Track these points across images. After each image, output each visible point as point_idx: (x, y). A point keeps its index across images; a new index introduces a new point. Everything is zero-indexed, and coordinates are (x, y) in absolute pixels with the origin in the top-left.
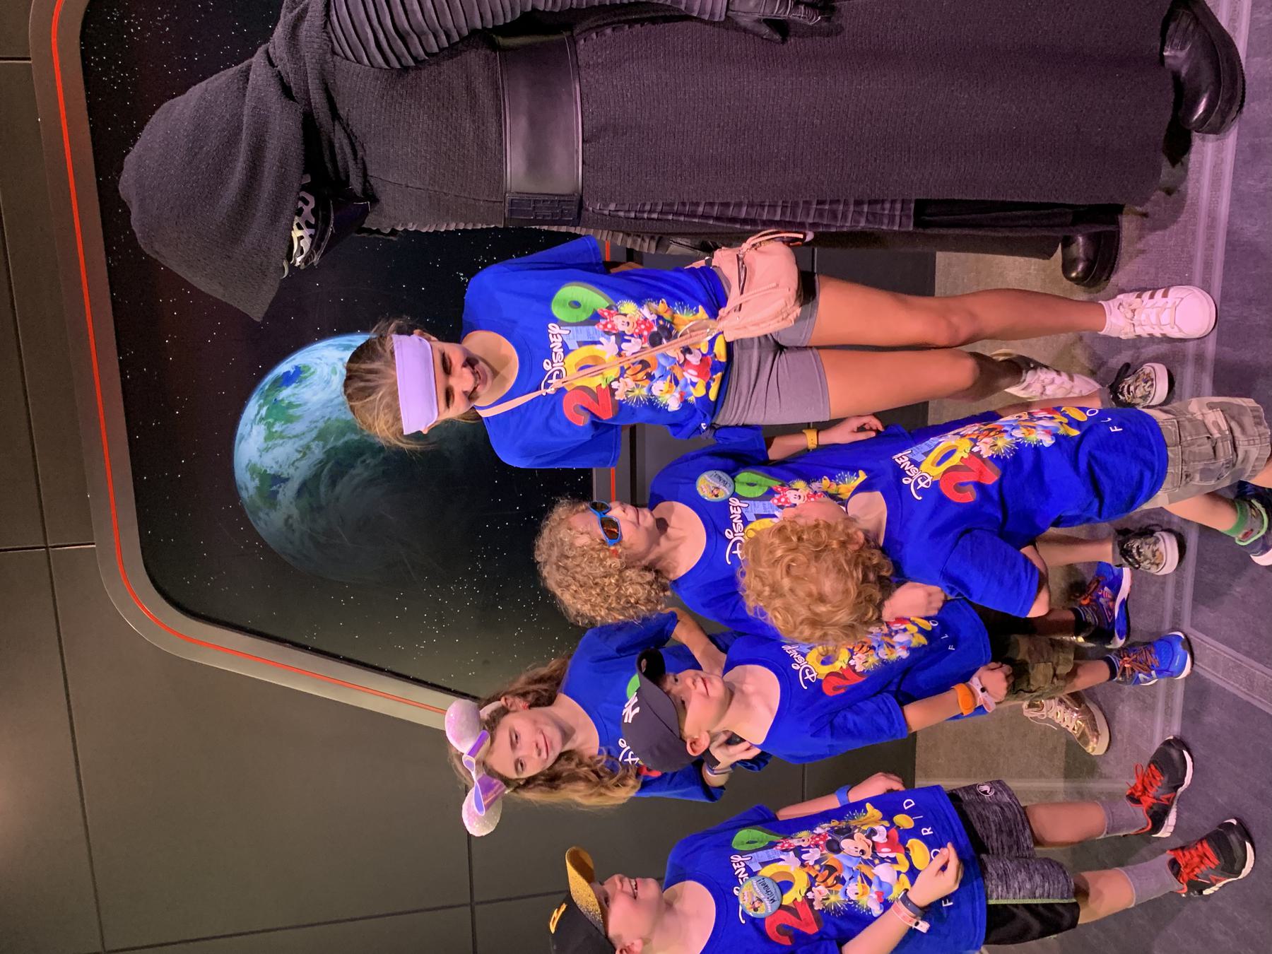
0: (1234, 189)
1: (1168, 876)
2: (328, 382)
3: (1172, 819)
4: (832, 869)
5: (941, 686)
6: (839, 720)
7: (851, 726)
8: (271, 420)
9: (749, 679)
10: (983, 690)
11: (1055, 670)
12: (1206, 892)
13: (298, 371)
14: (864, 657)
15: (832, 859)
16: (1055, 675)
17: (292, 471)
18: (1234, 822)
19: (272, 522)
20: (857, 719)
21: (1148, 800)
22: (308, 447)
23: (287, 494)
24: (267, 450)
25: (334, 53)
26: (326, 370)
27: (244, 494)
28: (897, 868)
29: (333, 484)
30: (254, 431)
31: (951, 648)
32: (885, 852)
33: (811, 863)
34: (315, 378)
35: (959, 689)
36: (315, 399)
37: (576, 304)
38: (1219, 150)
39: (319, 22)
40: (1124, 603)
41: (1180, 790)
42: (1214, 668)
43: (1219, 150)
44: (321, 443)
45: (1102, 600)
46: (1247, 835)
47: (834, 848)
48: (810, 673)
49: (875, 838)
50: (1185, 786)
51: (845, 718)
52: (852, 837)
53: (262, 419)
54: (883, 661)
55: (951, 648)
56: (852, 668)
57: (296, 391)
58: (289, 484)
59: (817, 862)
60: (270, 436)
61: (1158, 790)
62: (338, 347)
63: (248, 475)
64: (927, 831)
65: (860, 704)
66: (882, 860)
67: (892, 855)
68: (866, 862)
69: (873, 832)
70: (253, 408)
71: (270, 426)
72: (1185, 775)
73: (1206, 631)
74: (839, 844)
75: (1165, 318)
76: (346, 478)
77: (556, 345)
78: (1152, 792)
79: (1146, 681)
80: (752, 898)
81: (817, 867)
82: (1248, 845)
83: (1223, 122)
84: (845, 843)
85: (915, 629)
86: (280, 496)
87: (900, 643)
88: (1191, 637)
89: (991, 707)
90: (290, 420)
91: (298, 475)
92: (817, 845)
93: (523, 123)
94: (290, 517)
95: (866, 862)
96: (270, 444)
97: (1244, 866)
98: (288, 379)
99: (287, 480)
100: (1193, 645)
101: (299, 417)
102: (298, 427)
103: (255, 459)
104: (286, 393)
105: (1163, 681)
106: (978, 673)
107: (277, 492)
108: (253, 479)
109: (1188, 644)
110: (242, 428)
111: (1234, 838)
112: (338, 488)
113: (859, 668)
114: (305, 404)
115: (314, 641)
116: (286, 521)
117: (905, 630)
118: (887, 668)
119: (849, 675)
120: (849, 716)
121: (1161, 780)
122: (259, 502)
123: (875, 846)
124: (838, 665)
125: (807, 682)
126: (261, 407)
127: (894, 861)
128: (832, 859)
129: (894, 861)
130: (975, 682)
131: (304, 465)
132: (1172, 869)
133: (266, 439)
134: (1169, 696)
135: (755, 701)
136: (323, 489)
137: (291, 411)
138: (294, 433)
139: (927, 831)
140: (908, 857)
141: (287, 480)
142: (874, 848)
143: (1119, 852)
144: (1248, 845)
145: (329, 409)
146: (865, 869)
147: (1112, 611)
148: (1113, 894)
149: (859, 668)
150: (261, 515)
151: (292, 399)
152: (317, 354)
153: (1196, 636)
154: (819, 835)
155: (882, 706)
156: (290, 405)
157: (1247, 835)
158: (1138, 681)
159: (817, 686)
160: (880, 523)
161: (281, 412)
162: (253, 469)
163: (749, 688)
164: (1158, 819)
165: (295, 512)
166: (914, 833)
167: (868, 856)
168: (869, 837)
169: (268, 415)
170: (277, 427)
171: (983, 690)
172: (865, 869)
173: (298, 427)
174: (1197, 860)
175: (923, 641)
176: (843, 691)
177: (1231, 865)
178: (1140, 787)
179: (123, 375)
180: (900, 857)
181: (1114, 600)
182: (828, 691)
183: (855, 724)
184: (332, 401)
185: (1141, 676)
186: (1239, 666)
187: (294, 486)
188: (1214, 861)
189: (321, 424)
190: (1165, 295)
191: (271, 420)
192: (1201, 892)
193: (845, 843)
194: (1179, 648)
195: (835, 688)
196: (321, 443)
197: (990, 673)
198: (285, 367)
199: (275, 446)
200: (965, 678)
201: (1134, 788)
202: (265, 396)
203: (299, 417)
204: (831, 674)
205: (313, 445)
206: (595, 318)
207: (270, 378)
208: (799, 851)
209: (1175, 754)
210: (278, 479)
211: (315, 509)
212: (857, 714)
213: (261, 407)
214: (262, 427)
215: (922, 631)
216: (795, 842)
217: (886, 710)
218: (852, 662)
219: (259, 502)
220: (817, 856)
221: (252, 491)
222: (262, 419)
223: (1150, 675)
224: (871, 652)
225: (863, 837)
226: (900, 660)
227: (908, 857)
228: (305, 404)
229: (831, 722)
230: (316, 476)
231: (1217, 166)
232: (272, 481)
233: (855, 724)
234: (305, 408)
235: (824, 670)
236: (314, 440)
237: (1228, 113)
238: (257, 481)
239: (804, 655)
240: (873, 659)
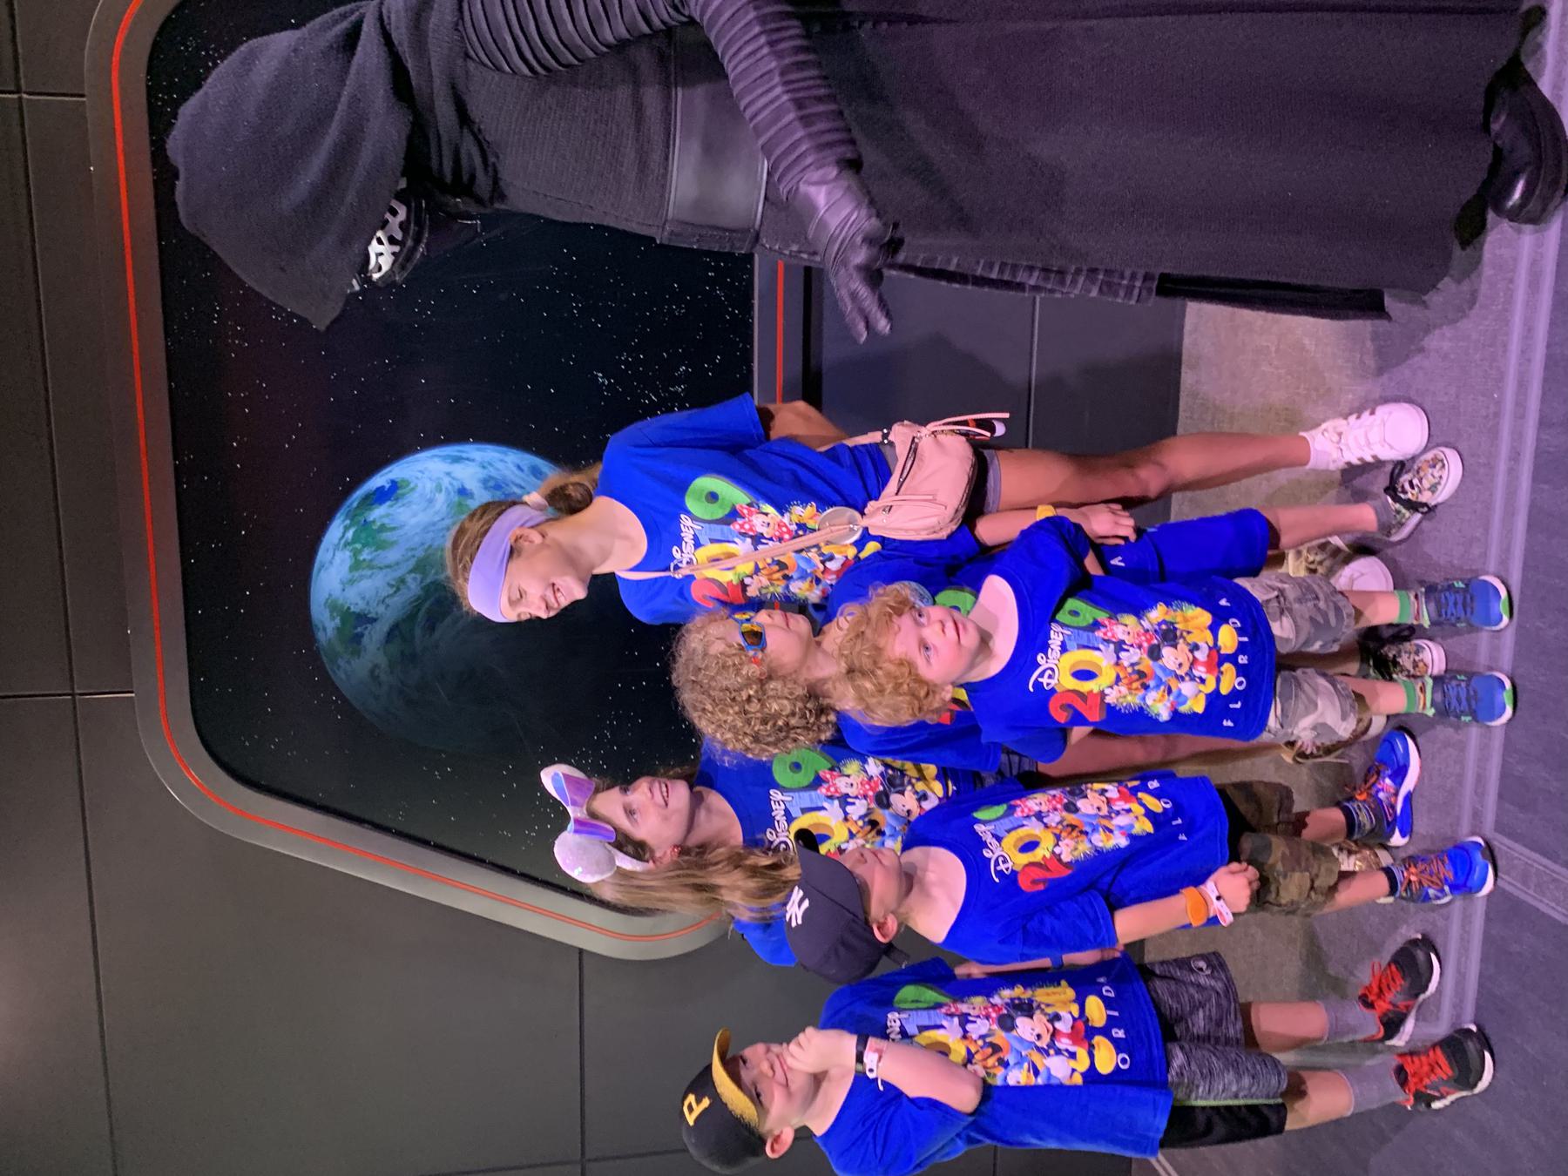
0: (1557, 292)
1: (1392, 1084)
2: (431, 501)
3: (1409, 1025)
4: (996, 1049)
5: (1167, 889)
6: (1033, 925)
7: (1047, 932)
8: (358, 546)
9: (931, 866)
10: (1218, 898)
11: (1312, 881)
12: (1436, 1105)
13: (395, 485)
14: (1072, 843)
15: (1000, 1037)
16: (1312, 888)
17: (381, 609)
18: (1474, 1028)
19: (357, 670)
20: (1056, 923)
21: (1382, 1006)
22: (402, 581)
23: (374, 637)
24: (352, 582)
25: (467, 56)
26: (429, 486)
27: (320, 636)
28: (1072, 1064)
29: (431, 626)
30: (337, 560)
31: (1183, 837)
32: (1064, 1043)
33: (974, 1036)
34: (414, 496)
35: (1189, 893)
36: (413, 521)
37: (713, 497)
38: (1539, 245)
39: (450, 18)
40: (1408, 798)
41: (1422, 997)
42: (1525, 883)
43: (1539, 245)
44: (419, 576)
45: (1381, 795)
46: (1485, 1042)
47: (1007, 1024)
48: (1005, 862)
49: (1058, 1025)
50: (1428, 993)
51: (1042, 922)
52: (1031, 1017)
53: (347, 544)
54: (1099, 851)
55: (1183, 837)
56: (1057, 857)
57: (391, 511)
58: (378, 626)
59: (982, 1037)
60: (356, 565)
61: (1395, 996)
62: (444, 458)
63: (327, 614)
64: (1119, 1033)
65: (1062, 905)
66: (1058, 1052)
67: (1072, 1049)
68: (1039, 1049)
69: (1056, 1017)
70: (337, 530)
71: (356, 553)
72: (1429, 980)
73: (1512, 835)
74: (1013, 1019)
75: (1375, 436)
76: (448, 620)
77: (687, 536)
78: (1389, 997)
79: (1438, 898)
80: (1058, 669)
81: (980, 1043)
82: (1487, 1055)
83: (1544, 210)
84: (1021, 1022)
85: (1142, 811)
86: (365, 640)
87: (1120, 827)
88: (1495, 844)
89: (1227, 918)
90: (381, 546)
91: (388, 615)
92: (988, 1017)
93: (696, 147)
94: (376, 666)
95: (1039, 1049)
96: (356, 574)
97: (1480, 1078)
98: (382, 496)
99: (375, 620)
100: (1496, 853)
101: (394, 543)
102: (392, 555)
103: (337, 592)
104: (378, 513)
105: (1459, 903)
106: (1213, 877)
107: (362, 635)
108: (333, 618)
109: (1490, 853)
110: (323, 554)
111: (1471, 1046)
112: (437, 634)
113: (1066, 858)
114: (402, 526)
115: (399, 822)
116: (372, 672)
117: (1129, 811)
118: (1101, 858)
119: (1054, 866)
120: (1048, 920)
121: (1401, 984)
122: (339, 648)
123: (1194, 662)
124: (1039, 854)
125: (1000, 873)
126: (346, 529)
127: (1073, 1055)
128: (1000, 1037)
129: (1203, 681)
130: (1210, 888)
131: (398, 600)
132: (1398, 1078)
133: (353, 568)
134: (1466, 919)
135: (936, 892)
136: (418, 632)
137: (384, 536)
138: (387, 562)
139: (1119, 1033)
140: (1091, 1056)
141: (375, 620)
142: (1053, 1035)
143: (1334, 1050)
144: (1487, 1055)
145: (431, 535)
146: (1037, 1058)
147: (1393, 807)
148: (1327, 1101)
149: (1066, 858)
150: (341, 662)
151: (386, 521)
152: (420, 466)
153: (1501, 843)
154: (993, 1006)
155: (1088, 909)
156: (383, 528)
157: (1485, 1042)
158: (1427, 898)
159: (1011, 878)
160: (1354, 1030)
161: (370, 536)
162: (334, 607)
163: (931, 876)
164: (1392, 1025)
165: (382, 660)
166: (1105, 1031)
167: (1043, 1044)
168: (1191, 651)
169: (355, 539)
170: (365, 555)
171: (1218, 898)
172: (1037, 1058)
173: (392, 555)
174: (1426, 1068)
175: (1149, 827)
176: (1041, 887)
177: (1467, 1076)
178: (1376, 990)
179: (178, 484)
180: (1082, 1053)
181: (1396, 794)
182: (1025, 884)
183: (1053, 930)
184: (434, 524)
185: (1431, 892)
186: (1554, 880)
187: (381, 629)
188: (1446, 1070)
189: (420, 553)
190: (1372, 413)
191: (358, 546)
192: (1429, 1106)
193: (1021, 1022)
194: (1479, 858)
195: (1034, 882)
196: (419, 576)
197: (1230, 878)
198: (379, 480)
199: (362, 577)
200: (1199, 880)
201: (1369, 988)
202: (352, 516)
203: (394, 543)
204: (1032, 864)
205: (409, 578)
206: (734, 514)
207: (359, 493)
208: (965, 1020)
209: (1420, 955)
210: (363, 619)
211: (408, 658)
212: (1058, 918)
213: (346, 529)
214: (348, 553)
215: (1149, 814)
216: (964, 1008)
217: (1092, 915)
218: (1057, 850)
219: (339, 648)
220: (984, 1031)
221: (330, 632)
222: (347, 544)
223: (1442, 891)
224: (1084, 837)
225: (1045, 1019)
226: (1117, 850)
227: (1091, 1056)
228: (402, 526)
229: (1024, 927)
230: (411, 617)
231: (1535, 263)
232: (355, 622)
233: (1053, 930)
234: (401, 532)
235: (1022, 860)
236: (411, 571)
237: (1552, 198)
238: (338, 621)
239: (999, 839)
240: (1084, 848)
